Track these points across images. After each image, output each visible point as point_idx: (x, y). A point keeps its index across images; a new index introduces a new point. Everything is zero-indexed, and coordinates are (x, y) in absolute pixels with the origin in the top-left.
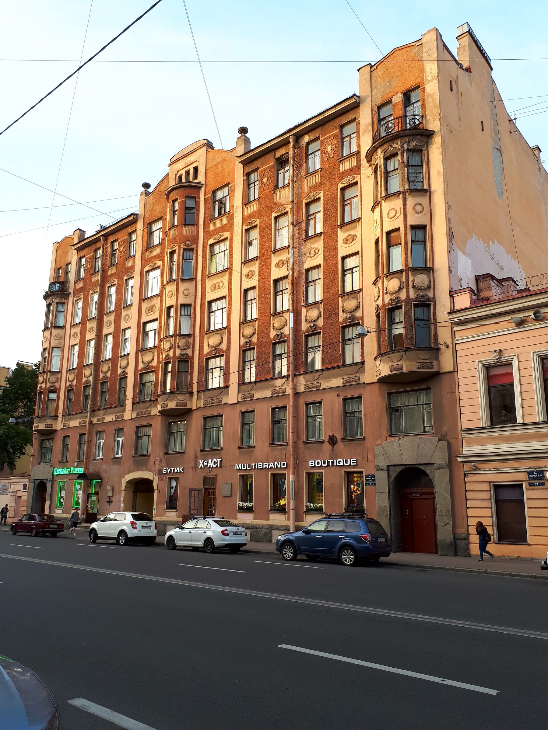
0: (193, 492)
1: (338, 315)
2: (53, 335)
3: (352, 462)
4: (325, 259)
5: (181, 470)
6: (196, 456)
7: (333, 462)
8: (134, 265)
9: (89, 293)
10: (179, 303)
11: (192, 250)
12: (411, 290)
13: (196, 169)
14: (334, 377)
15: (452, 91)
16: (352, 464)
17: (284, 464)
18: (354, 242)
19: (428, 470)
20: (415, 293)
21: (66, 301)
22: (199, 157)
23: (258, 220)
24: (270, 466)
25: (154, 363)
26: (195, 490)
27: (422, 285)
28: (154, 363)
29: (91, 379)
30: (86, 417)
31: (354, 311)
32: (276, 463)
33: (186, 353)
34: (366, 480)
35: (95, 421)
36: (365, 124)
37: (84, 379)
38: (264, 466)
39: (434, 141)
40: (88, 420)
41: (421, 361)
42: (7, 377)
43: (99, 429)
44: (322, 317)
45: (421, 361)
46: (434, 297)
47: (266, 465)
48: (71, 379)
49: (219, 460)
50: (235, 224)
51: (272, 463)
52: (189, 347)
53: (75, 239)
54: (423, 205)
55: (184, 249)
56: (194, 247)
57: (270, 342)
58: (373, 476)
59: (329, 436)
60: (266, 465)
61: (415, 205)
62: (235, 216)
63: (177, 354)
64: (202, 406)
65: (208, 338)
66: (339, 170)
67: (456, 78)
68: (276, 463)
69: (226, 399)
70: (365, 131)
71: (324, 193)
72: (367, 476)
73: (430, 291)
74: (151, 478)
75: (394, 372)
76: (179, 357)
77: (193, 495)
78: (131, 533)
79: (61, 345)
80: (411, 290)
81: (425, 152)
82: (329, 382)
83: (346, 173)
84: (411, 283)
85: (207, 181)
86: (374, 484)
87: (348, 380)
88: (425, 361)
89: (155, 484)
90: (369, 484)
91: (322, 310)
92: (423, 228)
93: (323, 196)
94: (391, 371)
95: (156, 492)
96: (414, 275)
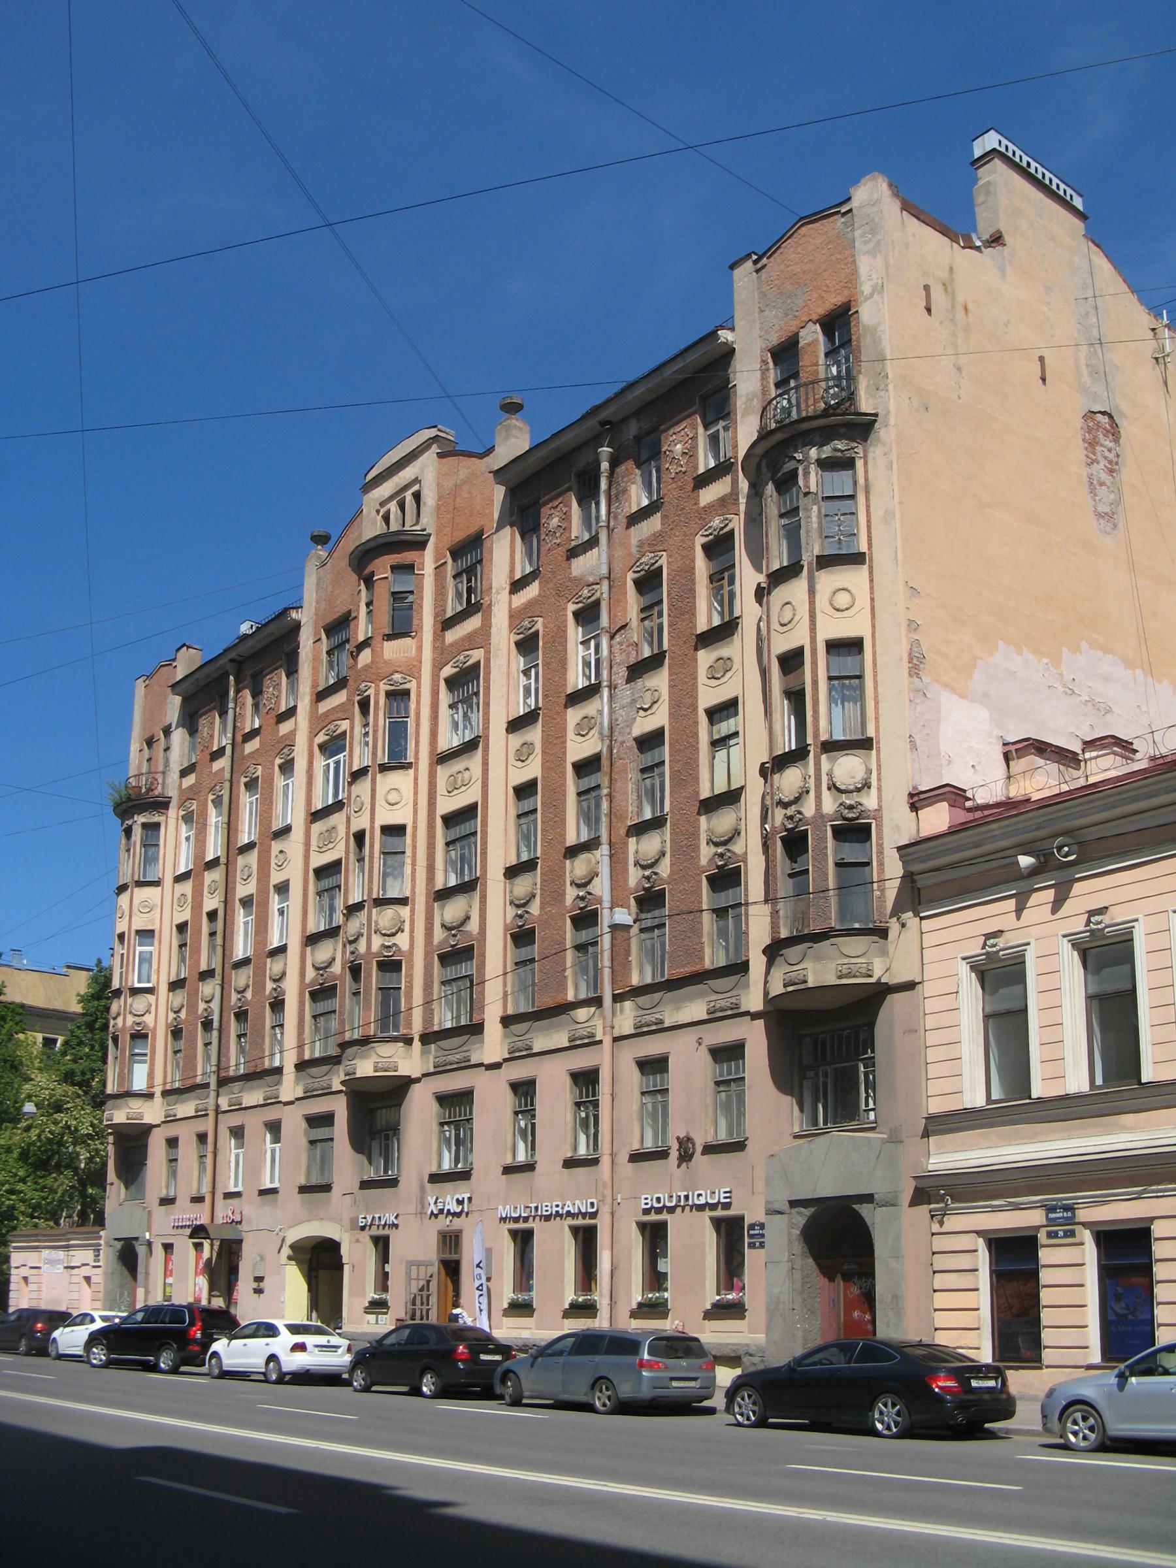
0: (414, 1269)
1: (696, 848)
2: (136, 901)
3: (723, 1195)
4: (672, 715)
5: (392, 1218)
6: (422, 1188)
7: (687, 1197)
8: (295, 730)
9: (206, 800)
10: (378, 824)
11: (407, 693)
12: (826, 795)
13: (417, 496)
14: (691, 998)
15: (929, 310)
16: (722, 1200)
17: (592, 1204)
18: (728, 675)
19: (864, 1210)
20: (835, 800)
21: (161, 819)
22: (422, 469)
23: (540, 620)
24: (566, 1209)
25: (337, 968)
26: (419, 1264)
27: (851, 781)
28: (337, 968)
29: (215, 1005)
30: (208, 1097)
31: (730, 839)
32: (577, 1202)
33: (395, 944)
34: (751, 1236)
35: (224, 1103)
36: (747, 395)
37: (202, 1006)
38: (555, 1209)
39: (878, 440)
40: (211, 1100)
41: (846, 961)
42: (78, 995)
43: (235, 1120)
44: (668, 855)
45: (846, 961)
46: (879, 809)
47: (557, 1206)
48: (176, 1005)
49: (466, 1196)
50: (493, 630)
51: (568, 1203)
52: (401, 930)
53: (179, 668)
54: (853, 591)
55: (389, 694)
56: (412, 686)
57: (564, 915)
58: (762, 1226)
59: (678, 1138)
60: (557, 1206)
61: (834, 593)
62: (495, 609)
63: (375, 947)
64: (432, 1070)
65: (442, 908)
66: (696, 504)
67: (945, 275)
68: (577, 1202)
69: (478, 1052)
70: (746, 412)
71: (669, 556)
72: (751, 1227)
73: (868, 794)
74: (336, 1238)
75: (790, 989)
76: (379, 954)
77: (414, 1275)
78: (293, 1362)
79: (153, 924)
80: (826, 795)
81: (859, 464)
82: (681, 1012)
83: (711, 509)
84: (824, 779)
85: (870, 476)
86: (762, 1245)
87: (718, 1006)
88: (853, 961)
89: (344, 1251)
90: (754, 1243)
91: (668, 837)
92: (854, 646)
93: (669, 563)
94: (785, 986)
95: (346, 1268)
96: (830, 760)
